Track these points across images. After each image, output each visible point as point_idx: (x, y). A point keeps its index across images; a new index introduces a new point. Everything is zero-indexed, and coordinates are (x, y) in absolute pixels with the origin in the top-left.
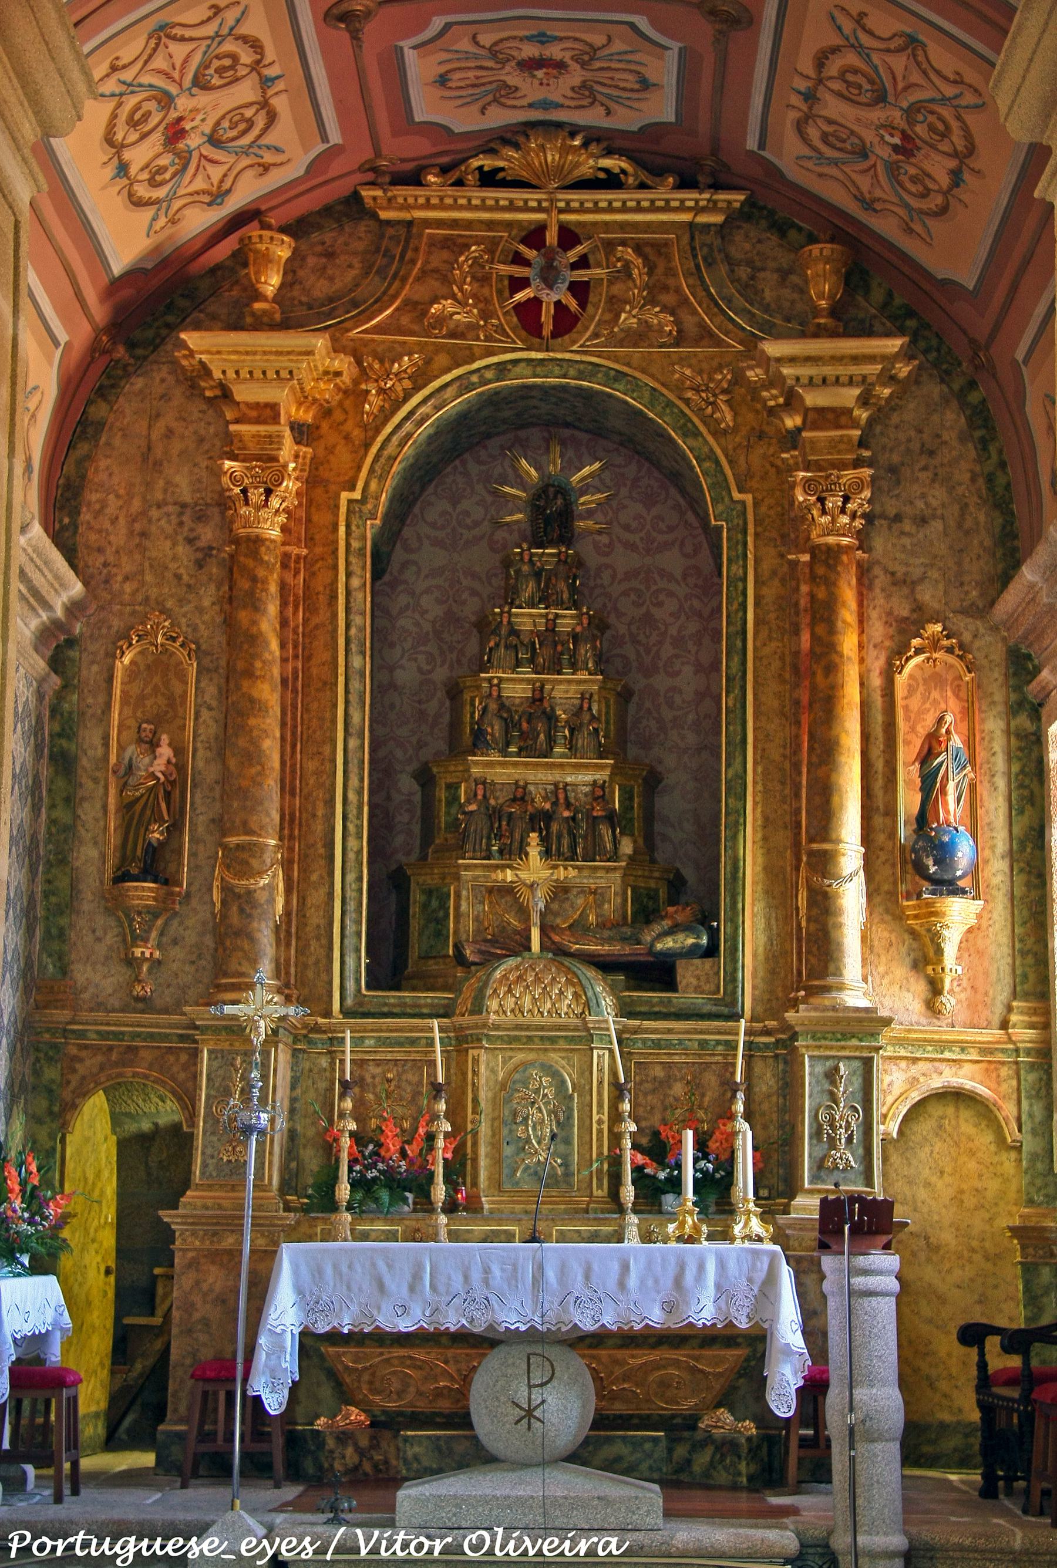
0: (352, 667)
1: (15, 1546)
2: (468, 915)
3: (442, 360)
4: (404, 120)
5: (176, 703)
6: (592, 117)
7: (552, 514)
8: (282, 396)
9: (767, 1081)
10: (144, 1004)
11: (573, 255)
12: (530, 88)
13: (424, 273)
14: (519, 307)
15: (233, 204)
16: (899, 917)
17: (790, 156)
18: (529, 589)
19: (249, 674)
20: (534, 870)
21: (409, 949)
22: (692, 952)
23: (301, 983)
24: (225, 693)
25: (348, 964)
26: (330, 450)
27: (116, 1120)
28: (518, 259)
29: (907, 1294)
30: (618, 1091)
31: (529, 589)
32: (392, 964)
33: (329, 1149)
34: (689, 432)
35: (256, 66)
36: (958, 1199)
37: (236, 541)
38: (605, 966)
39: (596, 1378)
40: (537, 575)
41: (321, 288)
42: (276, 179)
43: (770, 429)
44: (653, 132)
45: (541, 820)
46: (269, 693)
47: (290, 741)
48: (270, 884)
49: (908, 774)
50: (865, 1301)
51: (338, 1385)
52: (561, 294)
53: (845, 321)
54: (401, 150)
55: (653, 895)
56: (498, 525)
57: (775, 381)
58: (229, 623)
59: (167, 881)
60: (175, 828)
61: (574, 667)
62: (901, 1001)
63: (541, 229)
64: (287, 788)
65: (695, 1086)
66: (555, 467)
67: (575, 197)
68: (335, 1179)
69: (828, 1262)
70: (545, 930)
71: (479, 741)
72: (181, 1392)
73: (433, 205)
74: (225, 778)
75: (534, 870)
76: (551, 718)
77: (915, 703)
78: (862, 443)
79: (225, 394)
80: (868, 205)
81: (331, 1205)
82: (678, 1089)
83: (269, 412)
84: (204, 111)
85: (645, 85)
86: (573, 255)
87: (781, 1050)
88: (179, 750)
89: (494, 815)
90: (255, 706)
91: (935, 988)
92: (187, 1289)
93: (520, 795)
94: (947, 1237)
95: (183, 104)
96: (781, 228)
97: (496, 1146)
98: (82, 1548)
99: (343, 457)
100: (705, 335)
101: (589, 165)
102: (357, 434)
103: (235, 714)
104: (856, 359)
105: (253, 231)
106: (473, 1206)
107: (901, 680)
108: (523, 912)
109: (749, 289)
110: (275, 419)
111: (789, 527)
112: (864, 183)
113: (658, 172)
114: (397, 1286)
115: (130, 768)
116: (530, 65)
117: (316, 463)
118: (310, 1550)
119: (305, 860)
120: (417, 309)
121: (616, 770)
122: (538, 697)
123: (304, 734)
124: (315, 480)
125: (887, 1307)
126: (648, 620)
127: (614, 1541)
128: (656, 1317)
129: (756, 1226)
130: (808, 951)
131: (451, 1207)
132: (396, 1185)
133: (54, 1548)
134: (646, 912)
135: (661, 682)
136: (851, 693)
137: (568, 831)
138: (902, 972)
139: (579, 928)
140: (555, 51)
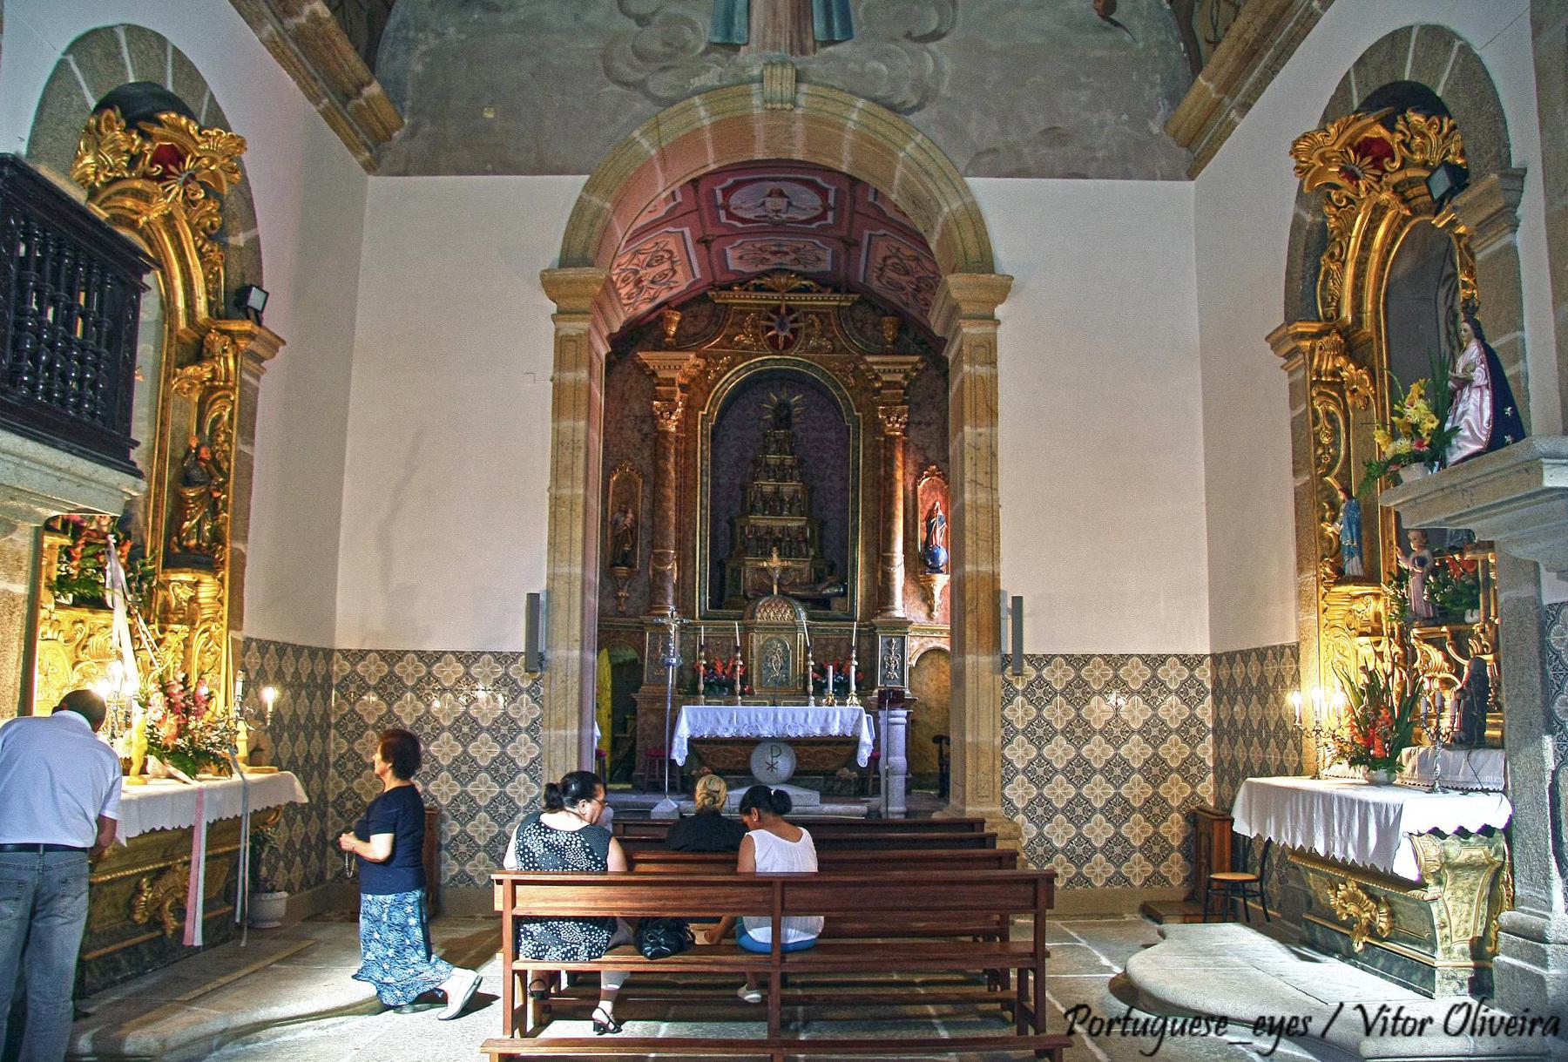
2: (749, 577)
3: (739, 358)
4: (725, 268)
5: (634, 496)
6: (800, 268)
7: (783, 416)
8: (678, 376)
9: (866, 644)
10: (623, 614)
11: (792, 318)
12: (775, 260)
16: (917, 580)
17: (875, 285)
18: (773, 447)
20: (775, 562)
21: (729, 595)
22: (838, 594)
23: (685, 609)
24: (654, 492)
25: (701, 599)
27: (610, 657)
28: (769, 319)
29: (911, 723)
30: (807, 650)
31: (773, 447)
32: (719, 599)
33: (695, 671)
34: (838, 388)
36: (937, 690)
38: (801, 600)
39: (797, 757)
40: (777, 442)
41: (692, 330)
42: (675, 291)
43: (867, 387)
44: (825, 273)
45: (777, 542)
46: (671, 494)
47: (679, 510)
48: (672, 567)
49: (921, 525)
50: (1328, 1035)
51: (700, 758)
52: (786, 333)
53: (899, 348)
54: (722, 278)
55: (822, 571)
56: (760, 419)
57: (871, 370)
58: (655, 463)
59: (631, 566)
60: (634, 546)
62: (918, 615)
63: (779, 307)
64: (678, 530)
65: (837, 648)
66: (784, 396)
67: (792, 296)
68: (697, 682)
69: (881, 713)
70: (779, 585)
71: (753, 510)
72: (640, 759)
73: (736, 297)
74: (653, 526)
75: (775, 562)
76: (782, 500)
79: (654, 374)
80: (906, 304)
81: (696, 692)
82: (831, 648)
83: (671, 382)
85: (819, 259)
86: (792, 318)
87: (869, 634)
88: (635, 514)
89: (759, 539)
91: (931, 609)
92: (645, 721)
93: (770, 530)
94: (933, 704)
95: (642, 272)
96: (874, 308)
97: (760, 670)
99: (700, 397)
101: (797, 284)
103: (657, 501)
104: (902, 364)
105: (664, 309)
106: (751, 693)
108: (771, 578)
109: (861, 331)
111: (877, 427)
113: (825, 286)
114: (724, 722)
115: (617, 522)
116: (775, 253)
117: (689, 399)
119: (685, 559)
120: (729, 338)
121: (808, 521)
122: (777, 492)
123: (685, 508)
124: (687, 407)
125: (902, 729)
126: (821, 460)
128: (818, 732)
129: (855, 700)
130: (881, 595)
131: (742, 693)
132: (722, 685)
134: (819, 579)
135: (827, 484)
136: (900, 494)
137: (788, 545)
138: (918, 602)
139: (793, 585)
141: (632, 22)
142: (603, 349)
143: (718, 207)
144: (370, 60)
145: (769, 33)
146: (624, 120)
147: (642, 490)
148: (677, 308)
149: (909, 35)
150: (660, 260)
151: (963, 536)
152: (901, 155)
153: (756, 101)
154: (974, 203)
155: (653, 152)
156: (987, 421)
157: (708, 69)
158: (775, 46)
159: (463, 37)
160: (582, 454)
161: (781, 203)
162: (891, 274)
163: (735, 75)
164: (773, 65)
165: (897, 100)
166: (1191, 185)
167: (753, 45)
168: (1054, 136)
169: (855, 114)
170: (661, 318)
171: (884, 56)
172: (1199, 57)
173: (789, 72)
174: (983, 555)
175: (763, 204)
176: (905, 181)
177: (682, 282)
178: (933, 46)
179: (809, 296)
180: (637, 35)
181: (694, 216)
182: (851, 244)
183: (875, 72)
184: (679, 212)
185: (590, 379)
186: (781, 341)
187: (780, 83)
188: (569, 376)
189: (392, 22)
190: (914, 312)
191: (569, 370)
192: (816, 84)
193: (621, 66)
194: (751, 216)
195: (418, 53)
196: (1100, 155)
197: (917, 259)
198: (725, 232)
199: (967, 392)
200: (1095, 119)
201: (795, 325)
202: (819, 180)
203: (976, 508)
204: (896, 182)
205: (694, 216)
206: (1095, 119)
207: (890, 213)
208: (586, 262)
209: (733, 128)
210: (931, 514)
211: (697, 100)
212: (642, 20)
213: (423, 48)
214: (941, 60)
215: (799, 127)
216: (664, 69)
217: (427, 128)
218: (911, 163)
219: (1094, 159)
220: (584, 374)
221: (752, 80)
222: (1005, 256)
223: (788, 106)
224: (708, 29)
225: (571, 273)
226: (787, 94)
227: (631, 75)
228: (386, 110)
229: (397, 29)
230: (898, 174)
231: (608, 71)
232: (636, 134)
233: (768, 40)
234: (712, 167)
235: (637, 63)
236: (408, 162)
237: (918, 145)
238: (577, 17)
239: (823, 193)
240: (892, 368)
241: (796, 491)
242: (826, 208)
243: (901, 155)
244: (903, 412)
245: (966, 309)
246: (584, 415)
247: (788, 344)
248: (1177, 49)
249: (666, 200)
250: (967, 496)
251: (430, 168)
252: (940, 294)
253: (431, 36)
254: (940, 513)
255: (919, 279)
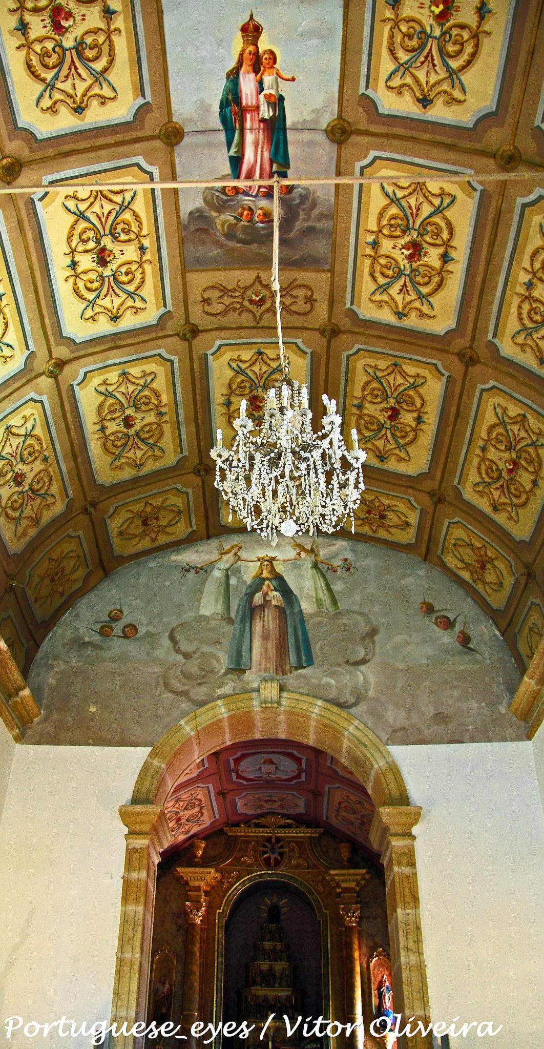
0: (218, 961)
1: (10, 1029)
4: (235, 812)
7: (274, 914)
8: (202, 884)
11: (279, 845)
12: (267, 806)
13: (240, 849)
14: (265, 859)
15: (190, 834)
17: (334, 822)
18: (268, 936)
19: (191, 963)
26: (214, 898)
28: (265, 846)
31: (268, 936)
35: (199, 805)
37: (189, 925)
40: (270, 932)
42: (202, 827)
46: (196, 969)
47: (202, 983)
49: (374, 993)
57: (333, 880)
58: (186, 947)
60: (169, 1009)
61: (281, 960)
63: (271, 838)
64: (201, 997)
66: (275, 901)
71: (254, 983)
73: (243, 832)
76: (274, 975)
77: (376, 972)
78: (358, 896)
79: (187, 883)
83: (198, 889)
84: (185, 814)
85: (297, 805)
86: (279, 845)
88: (171, 985)
90: (193, 973)
93: (266, 999)
95: (181, 814)
98: (64, 1032)
100: (315, 866)
102: (222, 894)
103: (186, 974)
107: (372, 964)
110: (200, 891)
111: (339, 920)
112: (354, 830)
116: (267, 801)
118: (247, 1032)
120: (238, 859)
122: (271, 969)
127: (490, 1024)
133: (41, 1030)
136: (358, 969)
140: (274, 799)
141: (181, 657)
142: (157, 860)
143: (231, 771)
144: (25, 672)
145: (264, 663)
146: (175, 714)
147: (176, 967)
148: (204, 839)
149: (347, 662)
150: (193, 806)
151: (402, 989)
152: (346, 733)
153: (256, 703)
154: (393, 761)
155: (192, 733)
156: (412, 904)
157: (226, 684)
158: (266, 670)
159: (80, 664)
160: (140, 929)
161: (271, 768)
162: (344, 814)
163: (243, 687)
164: (266, 681)
165: (342, 700)
166: (529, 744)
167: (253, 670)
168: (440, 718)
169: (317, 709)
170: (192, 846)
171: (332, 675)
172: (524, 664)
173: (275, 686)
174: (417, 1004)
175: (260, 769)
176: (349, 748)
177: (206, 821)
178: (362, 668)
179: (290, 830)
180: (184, 664)
181: (217, 776)
182: (317, 794)
183: (328, 684)
184: (207, 773)
185: (145, 876)
186: (272, 861)
187: (271, 691)
188: (134, 875)
189: (39, 655)
190: (360, 839)
191: (134, 871)
192: (293, 692)
193: (174, 682)
194: (252, 777)
195: (53, 673)
196: (470, 728)
197: (360, 803)
198: (235, 787)
199: (397, 885)
200: (465, 706)
201: (281, 850)
202: (295, 753)
203: (409, 967)
204: (344, 751)
205: (217, 776)
206: (465, 706)
207: (341, 773)
208: (147, 801)
209: (241, 720)
210: (381, 984)
211: (220, 702)
212: (187, 656)
213: (56, 670)
214: (368, 676)
215: (282, 718)
216: (200, 684)
217: (55, 716)
218: (352, 738)
219: (467, 731)
220: (144, 874)
221: (253, 690)
222: (416, 791)
223: (275, 705)
224: (226, 661)
225: (139, 808)
226: (275, 698)
227: (180, 688)
228: (32, 706)
229: (42, 659)
230: (344, 745)
231: (166, 685)
232: (182, 722)
233: (263, 666)
234: (229, 743)
235: (184, 680)
236: (41, 736)
237: (357, 727)
238: (148, 654)
239: (298, 761)
240: (348, 878)
241: (284, 969)
242: (300, 771)
243: (346, 733)
244: (357, 909)
245: (393, 829)
246: (142, 899)
247: (277, 863)
248: (511, 663)
249: (198, 764)
250: (403, 959)
251: (54, 740)
252: (375, 823)
253: (62, 663)
254: (387, 983)
255: (363, 816)
